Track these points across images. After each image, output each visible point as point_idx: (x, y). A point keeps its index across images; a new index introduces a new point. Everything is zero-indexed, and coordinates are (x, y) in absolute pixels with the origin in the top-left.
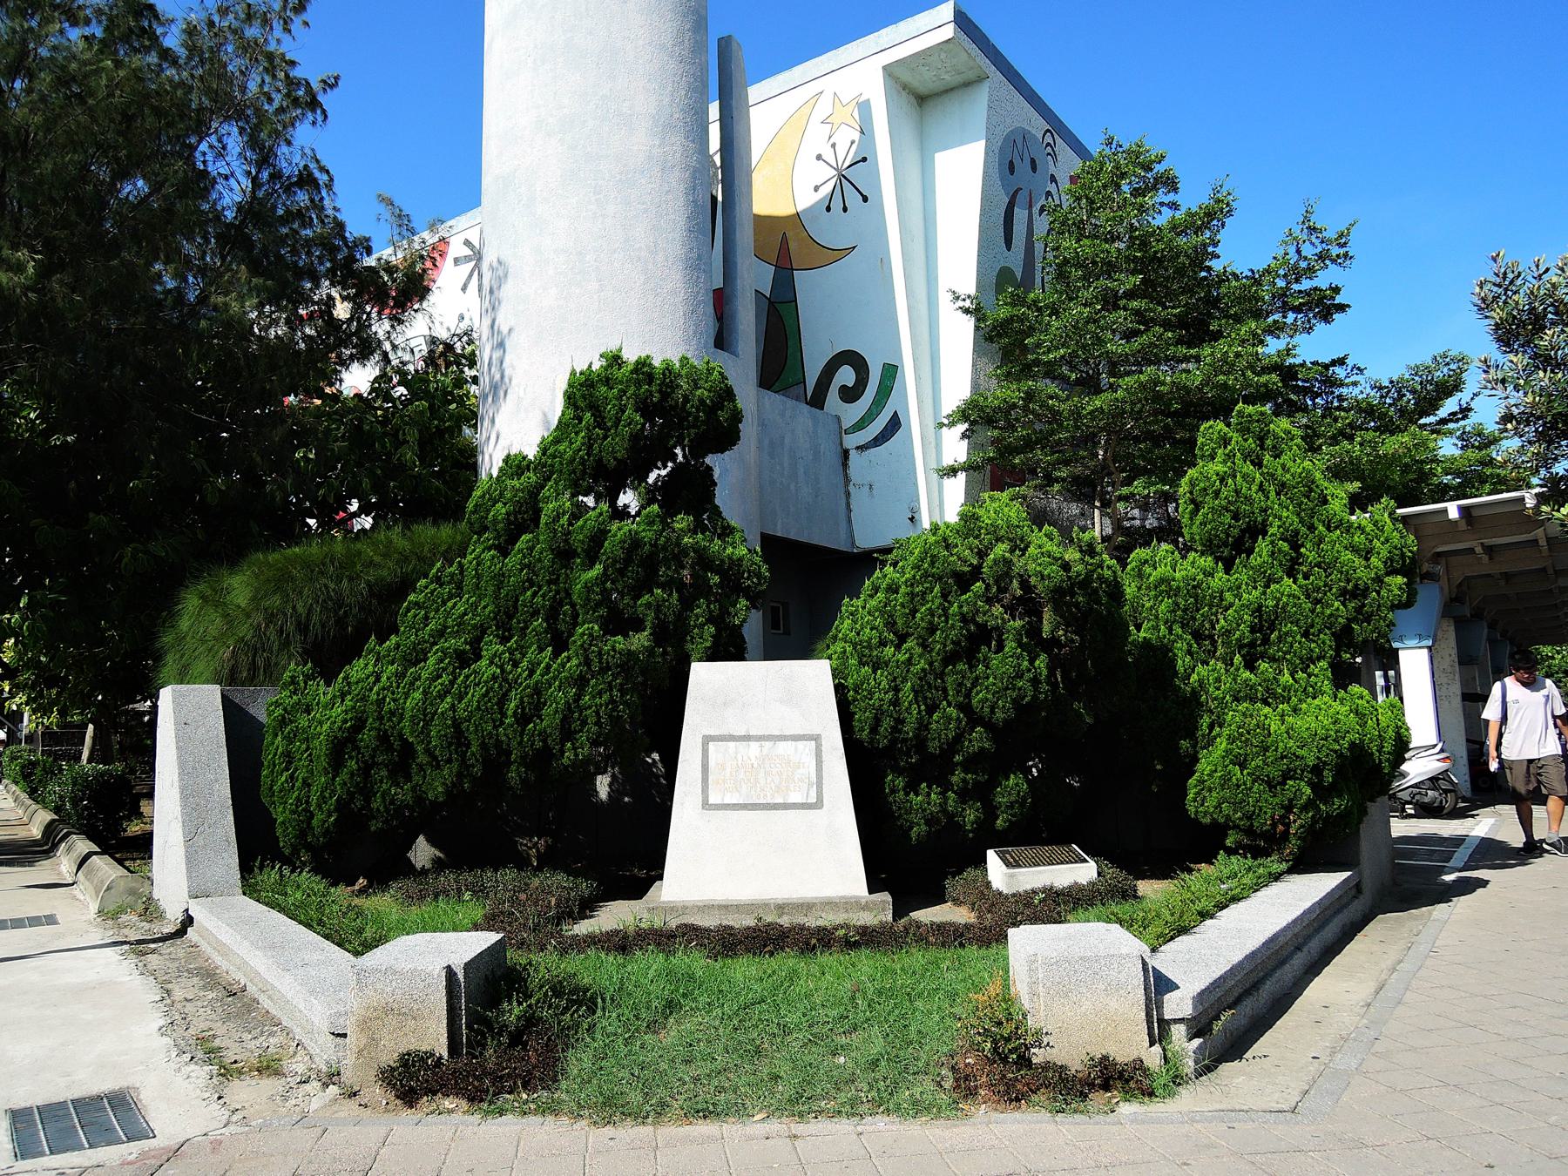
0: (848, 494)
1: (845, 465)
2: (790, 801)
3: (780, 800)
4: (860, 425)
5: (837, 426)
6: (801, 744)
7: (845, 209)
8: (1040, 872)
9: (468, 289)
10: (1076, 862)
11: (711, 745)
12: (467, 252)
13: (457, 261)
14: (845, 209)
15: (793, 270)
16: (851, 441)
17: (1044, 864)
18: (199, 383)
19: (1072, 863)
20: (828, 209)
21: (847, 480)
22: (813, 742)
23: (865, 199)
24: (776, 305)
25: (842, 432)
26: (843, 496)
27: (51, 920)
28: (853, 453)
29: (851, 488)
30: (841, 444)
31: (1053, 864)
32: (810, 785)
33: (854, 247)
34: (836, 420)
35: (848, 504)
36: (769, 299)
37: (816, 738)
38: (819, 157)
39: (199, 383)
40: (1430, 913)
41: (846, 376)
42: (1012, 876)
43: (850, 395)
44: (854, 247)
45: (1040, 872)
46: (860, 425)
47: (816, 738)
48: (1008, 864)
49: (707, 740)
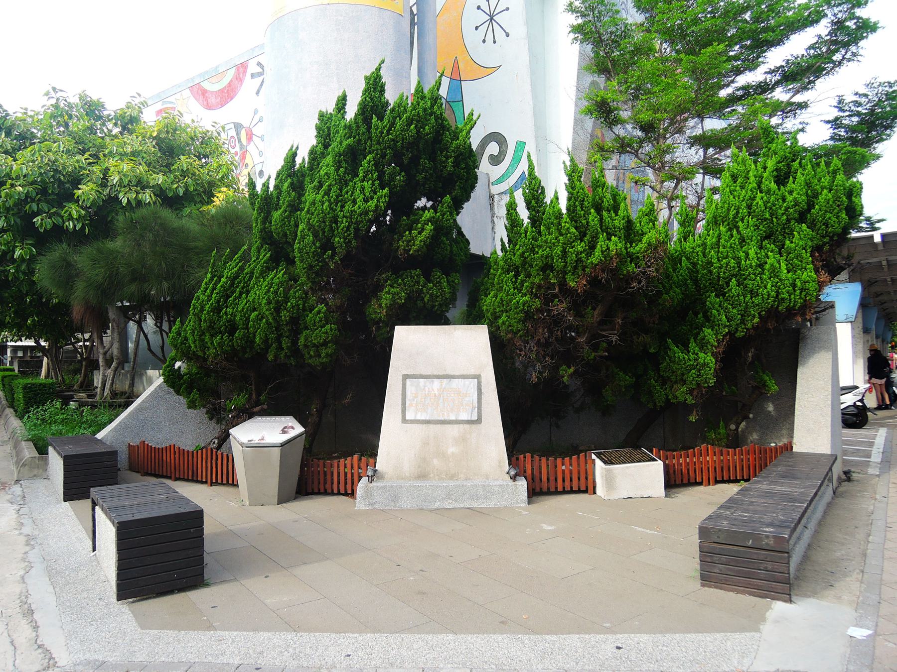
0: (493, 223)
1: (491, 205)
2: (460, 418)
3: (453, 418)
4: (500, 180)
5: (487, 180)
6: (467, 381)
7: (495, 42)
8: (627, 467)
9: (260, 93)
10: (649, 461)
11: (408, 382)
12: (259, 70)
13: (253, 76)
14: (495, 42)
15: (461, 81)
16: (495, 190)
17: (629, 463)
18: (374, 228)
19: (647, 461)
20: (484, 41)
21: (493, 215)
22: (476, 380)
23: (508, 35)
24: (451, 104)
25: (490, 184)
26: (490, 224)
27: (227, 455)
28: (496, 198)
29: (495, 219)
30: (490, 190)
31: (635, 462)
32: (473, 409)
33: (500, 66)
34: (487, 177)
35: (493, 229)
36: (446, 100)
37: (478, 377)
38: (479, 8)
39: (374, 228)
40: (771, 604)
41: (493, 148)
42: (608, 470)
43: (496, 160)
44: (500, 66)
45: (627, 467)
46: (500, 180)
47: (478, 377)
48: (605, 463)
49: (406, 377)
